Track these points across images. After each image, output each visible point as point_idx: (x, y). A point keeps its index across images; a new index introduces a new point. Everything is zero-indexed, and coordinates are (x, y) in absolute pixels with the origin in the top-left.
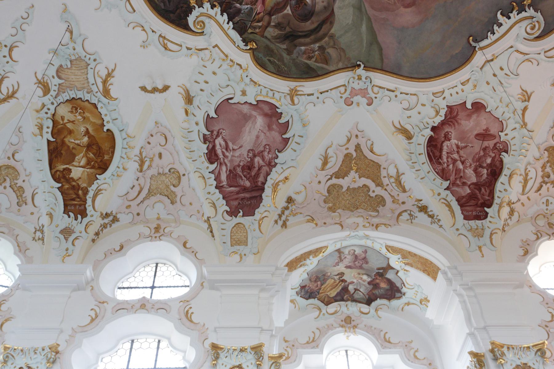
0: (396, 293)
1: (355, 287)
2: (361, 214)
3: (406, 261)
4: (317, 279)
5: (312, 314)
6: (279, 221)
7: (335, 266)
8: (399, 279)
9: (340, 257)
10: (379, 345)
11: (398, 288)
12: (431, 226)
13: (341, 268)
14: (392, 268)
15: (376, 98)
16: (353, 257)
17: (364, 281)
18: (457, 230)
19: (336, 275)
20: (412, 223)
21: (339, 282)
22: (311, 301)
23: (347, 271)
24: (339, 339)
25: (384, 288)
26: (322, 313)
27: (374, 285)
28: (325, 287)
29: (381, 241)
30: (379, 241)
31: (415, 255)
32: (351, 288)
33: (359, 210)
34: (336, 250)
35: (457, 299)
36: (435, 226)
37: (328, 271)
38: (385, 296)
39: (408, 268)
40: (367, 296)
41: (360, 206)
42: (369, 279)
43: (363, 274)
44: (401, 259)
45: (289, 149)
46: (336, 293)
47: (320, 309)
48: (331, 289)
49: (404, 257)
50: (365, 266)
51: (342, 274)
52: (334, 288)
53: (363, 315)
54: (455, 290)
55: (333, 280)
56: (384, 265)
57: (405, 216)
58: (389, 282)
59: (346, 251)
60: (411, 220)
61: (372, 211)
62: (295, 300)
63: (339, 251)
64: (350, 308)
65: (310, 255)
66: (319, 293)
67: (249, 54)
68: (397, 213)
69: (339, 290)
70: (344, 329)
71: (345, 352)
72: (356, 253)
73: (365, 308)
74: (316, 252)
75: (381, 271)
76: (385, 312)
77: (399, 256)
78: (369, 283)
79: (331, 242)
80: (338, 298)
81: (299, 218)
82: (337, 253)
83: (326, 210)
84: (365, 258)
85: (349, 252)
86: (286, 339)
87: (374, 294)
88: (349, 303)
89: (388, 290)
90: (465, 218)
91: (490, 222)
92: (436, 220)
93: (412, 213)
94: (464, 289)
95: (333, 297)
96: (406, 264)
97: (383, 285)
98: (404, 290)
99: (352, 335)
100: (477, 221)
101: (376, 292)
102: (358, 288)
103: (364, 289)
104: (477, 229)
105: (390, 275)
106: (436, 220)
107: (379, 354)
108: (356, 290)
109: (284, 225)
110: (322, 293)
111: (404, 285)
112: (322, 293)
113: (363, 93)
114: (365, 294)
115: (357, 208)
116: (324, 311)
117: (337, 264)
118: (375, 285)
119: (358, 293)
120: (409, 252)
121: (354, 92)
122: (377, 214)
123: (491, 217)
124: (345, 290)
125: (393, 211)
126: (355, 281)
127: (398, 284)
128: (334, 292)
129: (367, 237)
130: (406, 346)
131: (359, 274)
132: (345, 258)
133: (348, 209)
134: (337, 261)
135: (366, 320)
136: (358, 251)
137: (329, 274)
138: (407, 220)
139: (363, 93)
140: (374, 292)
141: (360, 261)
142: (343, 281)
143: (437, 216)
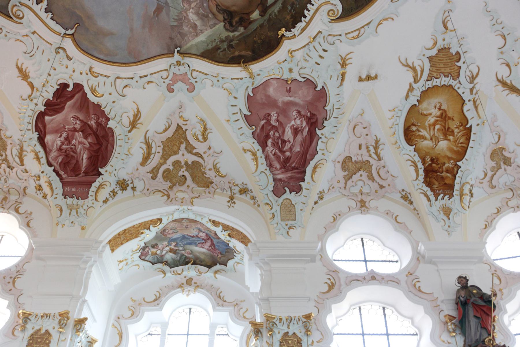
5: (157, 278)
15: (196, 82)
24: (178, 302)
29: (209, 211)
45: (115, 129)
67: (70, 39)
74: (147, 225)
113: (183, 78)
121: (176, 79)
139: (183, 78)
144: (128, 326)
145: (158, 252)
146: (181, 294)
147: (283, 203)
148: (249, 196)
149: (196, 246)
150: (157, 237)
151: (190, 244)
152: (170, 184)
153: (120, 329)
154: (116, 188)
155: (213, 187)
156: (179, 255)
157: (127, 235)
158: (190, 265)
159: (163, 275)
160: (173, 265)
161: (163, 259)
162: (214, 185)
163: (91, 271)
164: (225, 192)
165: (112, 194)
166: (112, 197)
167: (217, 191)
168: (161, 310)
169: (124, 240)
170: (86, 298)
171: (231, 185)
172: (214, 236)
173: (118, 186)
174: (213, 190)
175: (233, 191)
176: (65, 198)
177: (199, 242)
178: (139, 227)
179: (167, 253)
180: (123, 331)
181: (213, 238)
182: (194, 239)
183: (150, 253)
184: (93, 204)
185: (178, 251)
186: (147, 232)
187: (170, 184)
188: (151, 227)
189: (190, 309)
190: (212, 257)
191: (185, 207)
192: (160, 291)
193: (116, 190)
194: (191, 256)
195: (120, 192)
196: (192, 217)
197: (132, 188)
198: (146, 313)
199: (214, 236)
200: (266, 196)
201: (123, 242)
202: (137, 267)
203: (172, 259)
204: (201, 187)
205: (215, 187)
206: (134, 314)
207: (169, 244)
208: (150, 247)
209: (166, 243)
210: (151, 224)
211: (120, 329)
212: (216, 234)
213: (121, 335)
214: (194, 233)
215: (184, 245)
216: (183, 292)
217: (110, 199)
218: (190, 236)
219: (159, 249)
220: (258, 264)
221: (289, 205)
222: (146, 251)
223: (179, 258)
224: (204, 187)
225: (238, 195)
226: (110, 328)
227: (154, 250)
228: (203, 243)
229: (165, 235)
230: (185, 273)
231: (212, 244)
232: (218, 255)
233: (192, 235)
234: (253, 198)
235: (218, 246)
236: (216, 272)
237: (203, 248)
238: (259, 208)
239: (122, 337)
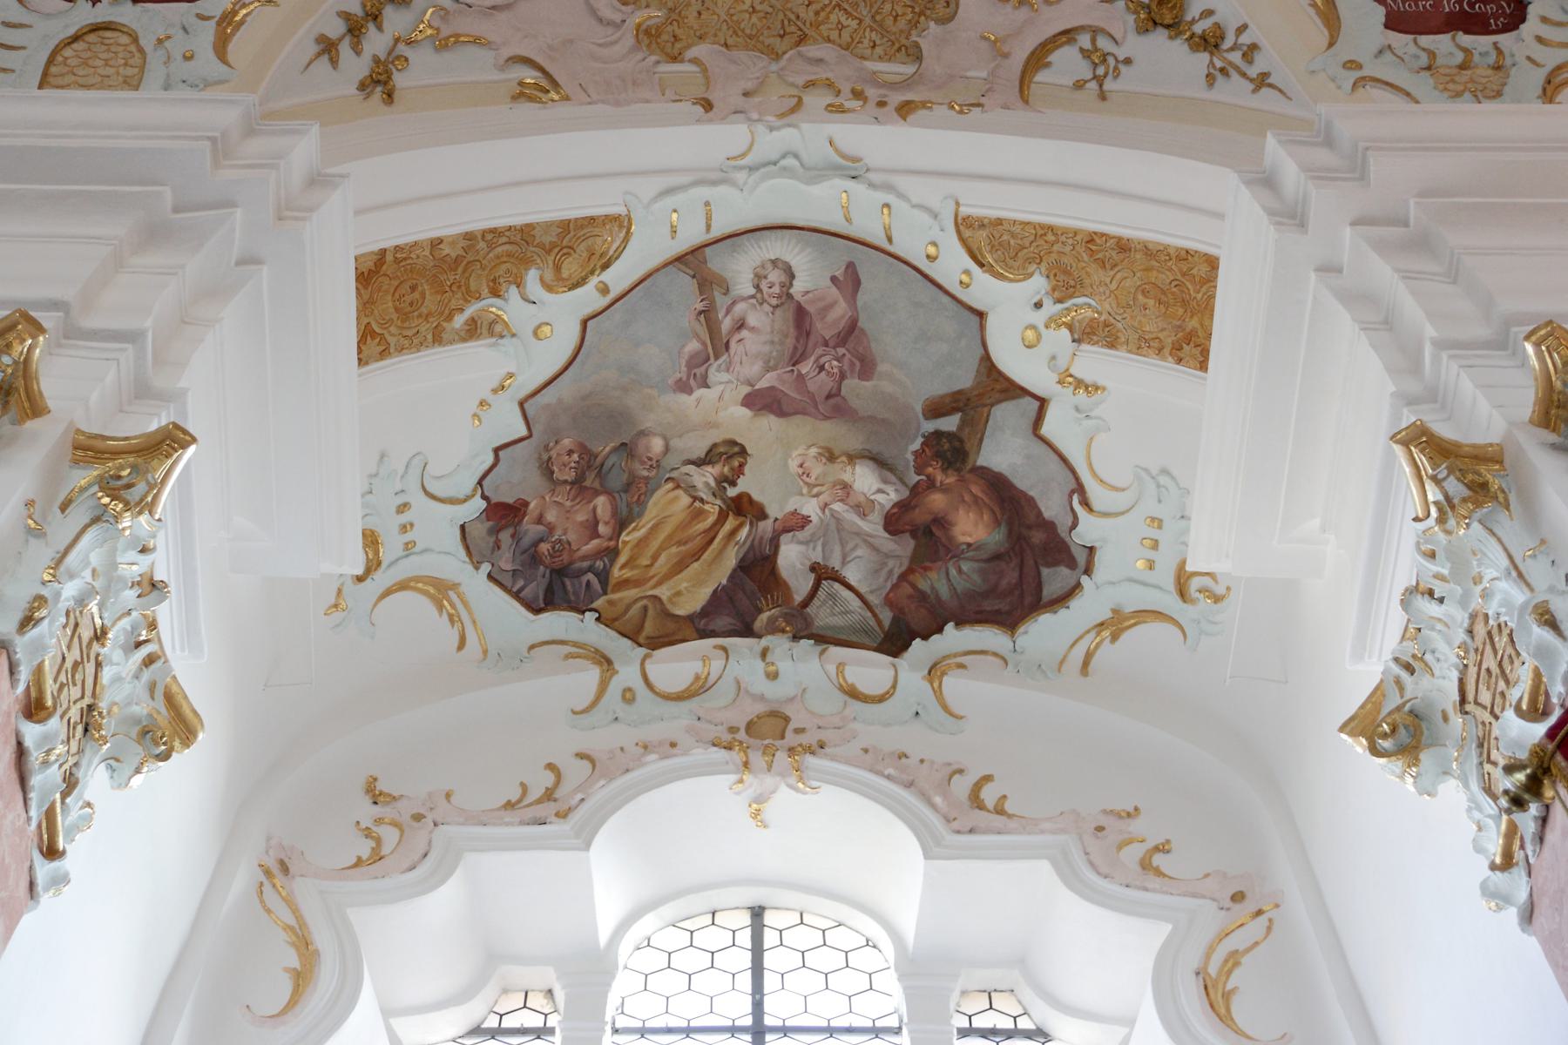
0: (1045, 572)
1: (817, 556)
2: (821, 73)
3: (1085, 306)
4: (587, 475)
6: (345, 49)
7: (683, 387)
8: (1054, 464)
9: (707, 315)
10: (936, 821)
11: (1050, 527)
12: (1213, 95)
13: (719, 407)
14: (1013, 390)
16: (784, 318)
17: (862, 509)
18: (1352, 65)
19: (699, 463)
20: (1103, 97)
21: (722, 517)
22: (558, 622)
23: (759, 432)
25: (982, 551)
26: (616, 685)
27: (919, 528)
28: (642, 543)
30: (918, 189)
31: (1123, 246)
32: (792, 558)
33: (812, 50)
34: (680, 259)
35: (1343, 323)
36: (1234, 91)
37: (649, 421)
38: (989, 605)
39: (1093, 362)
40: (886, 616)
41: (816, 25)
42: (891, 496)
43: (852, 458)
44: (1050, 308)
46: (705, 594)
47: (605, 662)
48: (680, 566)
49: (1065, 286)
50: (854, 388)
51: (731, 454)
52: (696, 555)
53: (857, 706)
54: (1329, 269)
55: (685, 500)
56: (964, 379)
57: (1067, 63)
58: (1005, 498)
59: (740, 269)
60: (1100, 80)
61: (887, 58)
62: (455, 586)
63: (691, 260)
64: (784, 666)
65: (527, 262)
66: (604, 577)
68: (1021, 53)
69: (721, 575)
70: (736, 756)
71: (745, 919)
72: (798, 287)
73: (868, 669)
75: (950, 423)
76: (987, 687)
77: (1038, 284)
78: (893, 523)
79: (647, 188)
80: (722, 622)
81: (473, 66)
82: (683, 283)
83: (629, 41)
84: (851, 331)
85: (759, 277)
86: (381, 786)
87: (922, 596)
88: (779, 644)
89: (997, 557)
90: (1395, 22)
91: (1539, 39)
92: (1236, 57)
93: (1103, 43)
94: (1381, 247)
95: (690, 618)
96: (1085, 334)
97: (972, 528)
98: (1088, 530)
99: (784, 789)
100: (1465, 39)
101: (939, 582)
102: (835, 562)
103: (866, 568)
104: (1463, 67)
105: (1002, 450)
106: (1236, 57)
107: (928, 855)
108: (822, 574)
109: (380, 82)
110: (624, 584)
111: (1085, 503)
112: (624, 584)
114: (874, 600)
115: (802, 40)
116: (627, 674)
117: (694, 376)
118: (928, 532)
119: (832, 596)
120: (1092, 238)
122: (909, 69)
123: (1544, 20)
124: (758, 570)
125: (998, 48)
126: (810, 508)
127: (1051, 507)
128: (698, 582)
129: (852, 168)
130: (1100, 829)
131: (831, 457)
132: (741, 325)
133: (753, 41)
134: (694, 346)
135: (870, 727)
136: (811, 275)
137: (657, 445)
138: (1079, 85)
140: (923, 585)
141: (823, 349)
142: (744, 507)
143: (1242, 29)
189: (757, 913)
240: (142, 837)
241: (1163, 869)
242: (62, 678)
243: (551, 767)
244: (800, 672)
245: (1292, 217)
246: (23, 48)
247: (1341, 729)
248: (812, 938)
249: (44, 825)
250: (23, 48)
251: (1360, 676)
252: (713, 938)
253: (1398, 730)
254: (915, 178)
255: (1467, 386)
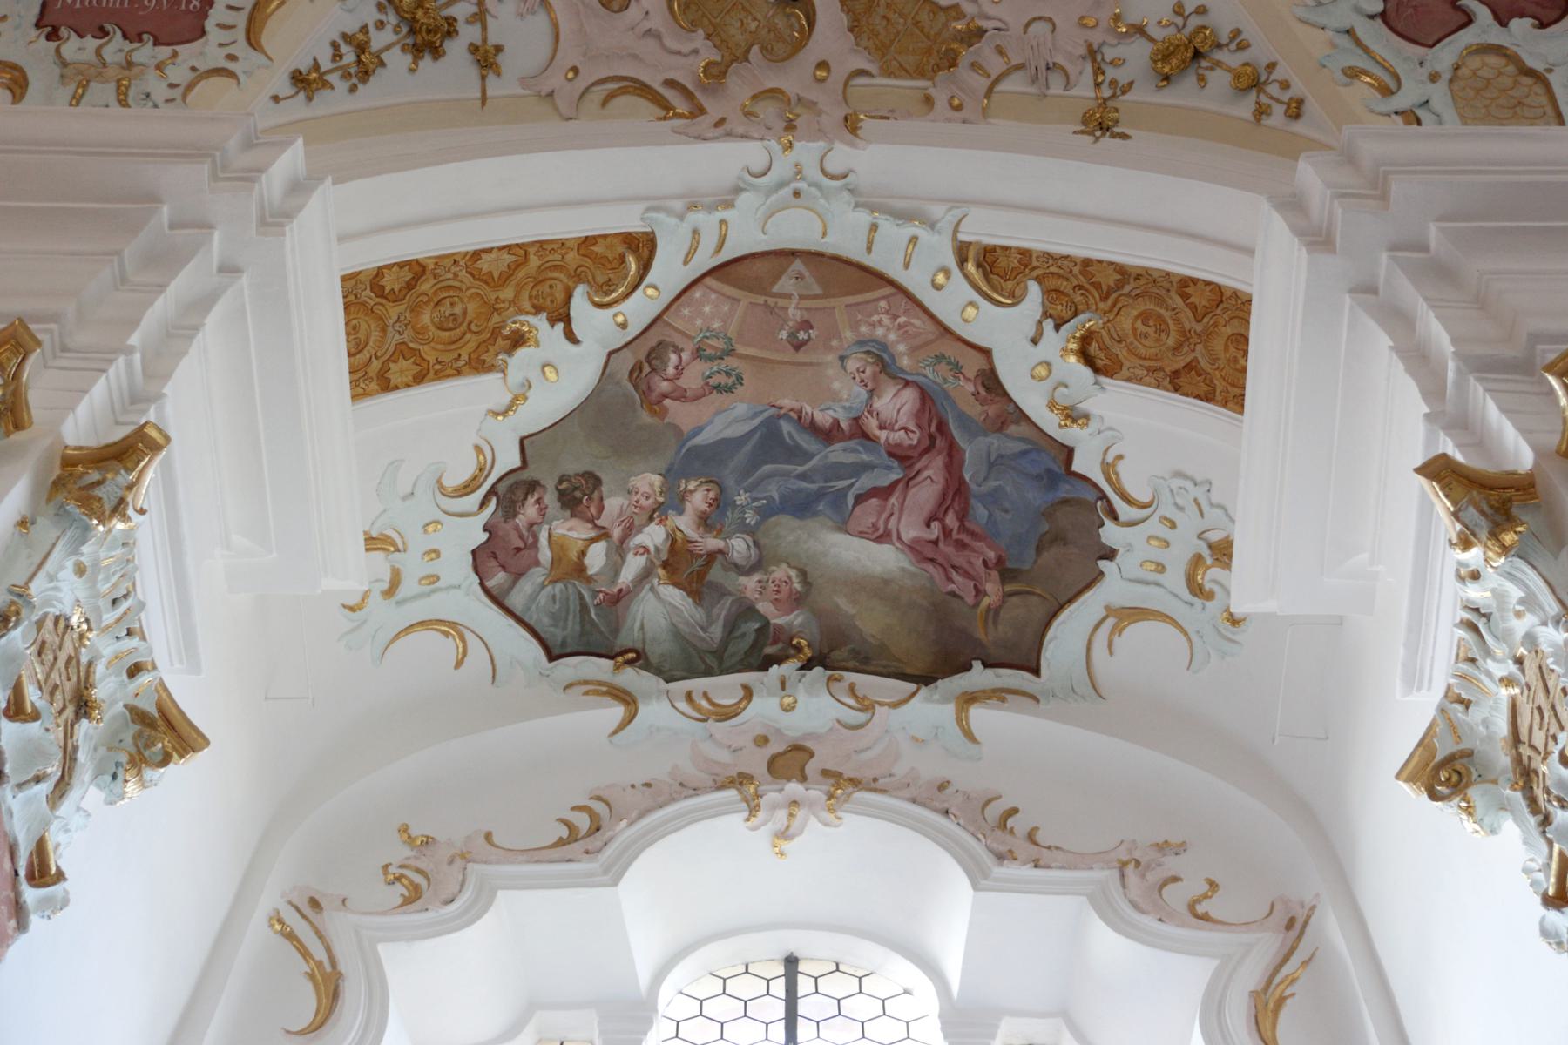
74: (548, 277)
144: (380, 947)
145: (596, 558)
146: (735, 822)
147: (1464, 71)
148: (1219, 80)
149: (843, 526)
150: (595, 413)
151: (801, 507)
152: (709, 54)
153: (319, 953)
154: (380, 25)
155: (975, 66)
156: (723, 609)
157: (426, 319)
158: (789, 668)
159: (617, 711)
160: (688, 661)
161: (616, 631)
162: (985, 49)
163: (196, 328)
164: (1056, 88)
165: (349, 57)
166: (346, 75)
167: (1003, 86)
168: (615, 882)
169: (402, 351)
170: (165, 391)
171: (1096, 37)
172: (974, 410)
173: (392, 18)
174: (983, 83)
175: (1111, 73)
176: (53, 35)
177: (865, 482)
178: (505, 278)
179: (645, 575)
180: (342, 967)
181: (963, 418)
182: (838, 453)
183: (545, 554)
184: (232, 58)
185: (716, 573)
186: (548, 334)
187: (709, 54)
188: (580, 304)
189: (791, 963)
190: (940, 611)
191: (806, 152)
192: (599, 807)
193: (378, 40)
194: (796, 619)
195: (398, 60)
196: (844, 233)
197: (473, 49)
198: (500, 893)
199: (974, 410)
200: (1345, 41)
201: (397, 371)
202: (447, 648)
203: (677, 634)
204: (904, 72)
205: (996, 65)
206: (427, 877)
207: (672, 501)
208: (550, 499)
209: (649, 482)
210: (579, 278)
211: (319, 953)
212: (991, 383)
213: (329, 987)
214: (837, 391)
215: (766, 513)
216: (753, 810)
217: (333, 78)
218: (813, 428)
219: (604, 534)
220: (1372, 290)
221: (1508, 82)
222: (521, 520)
223: (717, 631)
224: (920, 73)
225: (1144, 94)
226: (256, 934)
227: (573, 531)
228: (884, 493)
229: (655, 404)
230: (764, 708)
231: (955, 493)
232: (979, 592)
233: (823, 418)
234: (1252, 82)
235: (993, 498)
236: (968, 699)
237: (883, 537)
238: (1298, 127)
239: (335, 995)
240: (143, 867)
241: (1213, 914)
242: (55, 676)
243: (426, 532)
244: (807, 706)
245: (1319, 239)
246: (1111, 654)
247: (1398, 777)
248: (871, 1008)
249: (36, 861)
250: (1111, 654)
251: (1405, 718)
252: (746, 987)
253: (1446, 772)
254: (932, 195)
255: (1493, 413)
